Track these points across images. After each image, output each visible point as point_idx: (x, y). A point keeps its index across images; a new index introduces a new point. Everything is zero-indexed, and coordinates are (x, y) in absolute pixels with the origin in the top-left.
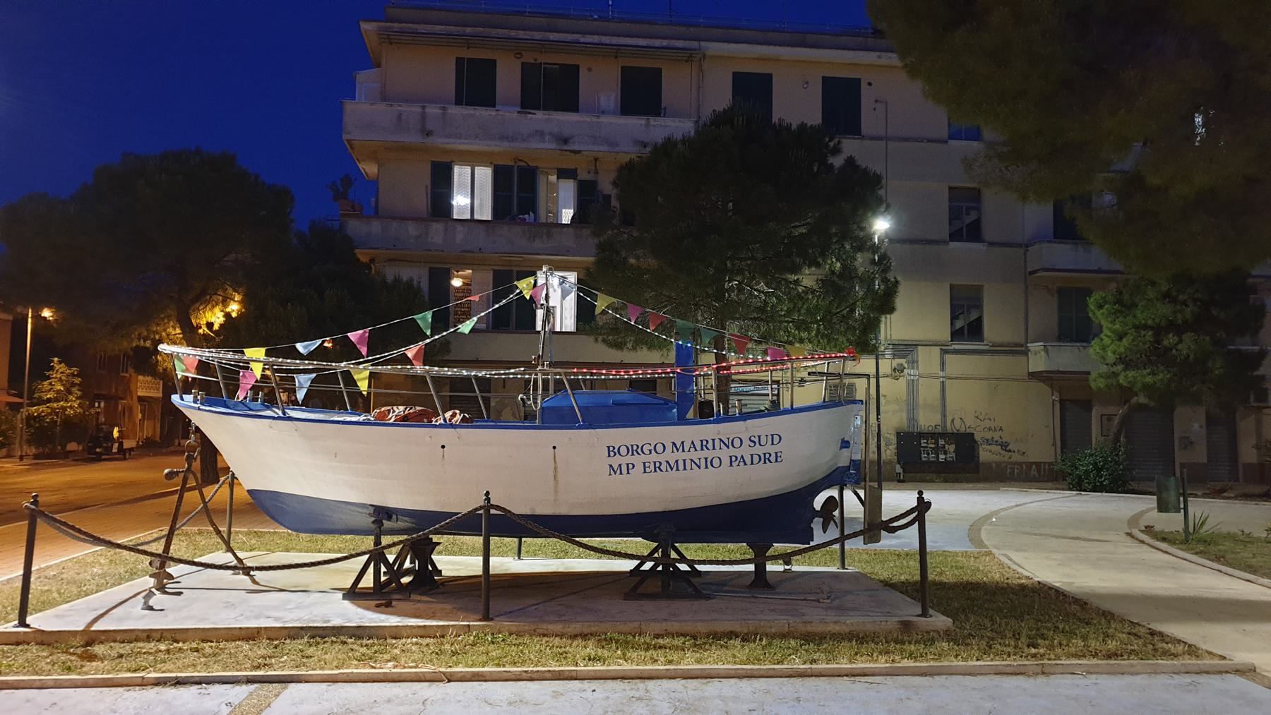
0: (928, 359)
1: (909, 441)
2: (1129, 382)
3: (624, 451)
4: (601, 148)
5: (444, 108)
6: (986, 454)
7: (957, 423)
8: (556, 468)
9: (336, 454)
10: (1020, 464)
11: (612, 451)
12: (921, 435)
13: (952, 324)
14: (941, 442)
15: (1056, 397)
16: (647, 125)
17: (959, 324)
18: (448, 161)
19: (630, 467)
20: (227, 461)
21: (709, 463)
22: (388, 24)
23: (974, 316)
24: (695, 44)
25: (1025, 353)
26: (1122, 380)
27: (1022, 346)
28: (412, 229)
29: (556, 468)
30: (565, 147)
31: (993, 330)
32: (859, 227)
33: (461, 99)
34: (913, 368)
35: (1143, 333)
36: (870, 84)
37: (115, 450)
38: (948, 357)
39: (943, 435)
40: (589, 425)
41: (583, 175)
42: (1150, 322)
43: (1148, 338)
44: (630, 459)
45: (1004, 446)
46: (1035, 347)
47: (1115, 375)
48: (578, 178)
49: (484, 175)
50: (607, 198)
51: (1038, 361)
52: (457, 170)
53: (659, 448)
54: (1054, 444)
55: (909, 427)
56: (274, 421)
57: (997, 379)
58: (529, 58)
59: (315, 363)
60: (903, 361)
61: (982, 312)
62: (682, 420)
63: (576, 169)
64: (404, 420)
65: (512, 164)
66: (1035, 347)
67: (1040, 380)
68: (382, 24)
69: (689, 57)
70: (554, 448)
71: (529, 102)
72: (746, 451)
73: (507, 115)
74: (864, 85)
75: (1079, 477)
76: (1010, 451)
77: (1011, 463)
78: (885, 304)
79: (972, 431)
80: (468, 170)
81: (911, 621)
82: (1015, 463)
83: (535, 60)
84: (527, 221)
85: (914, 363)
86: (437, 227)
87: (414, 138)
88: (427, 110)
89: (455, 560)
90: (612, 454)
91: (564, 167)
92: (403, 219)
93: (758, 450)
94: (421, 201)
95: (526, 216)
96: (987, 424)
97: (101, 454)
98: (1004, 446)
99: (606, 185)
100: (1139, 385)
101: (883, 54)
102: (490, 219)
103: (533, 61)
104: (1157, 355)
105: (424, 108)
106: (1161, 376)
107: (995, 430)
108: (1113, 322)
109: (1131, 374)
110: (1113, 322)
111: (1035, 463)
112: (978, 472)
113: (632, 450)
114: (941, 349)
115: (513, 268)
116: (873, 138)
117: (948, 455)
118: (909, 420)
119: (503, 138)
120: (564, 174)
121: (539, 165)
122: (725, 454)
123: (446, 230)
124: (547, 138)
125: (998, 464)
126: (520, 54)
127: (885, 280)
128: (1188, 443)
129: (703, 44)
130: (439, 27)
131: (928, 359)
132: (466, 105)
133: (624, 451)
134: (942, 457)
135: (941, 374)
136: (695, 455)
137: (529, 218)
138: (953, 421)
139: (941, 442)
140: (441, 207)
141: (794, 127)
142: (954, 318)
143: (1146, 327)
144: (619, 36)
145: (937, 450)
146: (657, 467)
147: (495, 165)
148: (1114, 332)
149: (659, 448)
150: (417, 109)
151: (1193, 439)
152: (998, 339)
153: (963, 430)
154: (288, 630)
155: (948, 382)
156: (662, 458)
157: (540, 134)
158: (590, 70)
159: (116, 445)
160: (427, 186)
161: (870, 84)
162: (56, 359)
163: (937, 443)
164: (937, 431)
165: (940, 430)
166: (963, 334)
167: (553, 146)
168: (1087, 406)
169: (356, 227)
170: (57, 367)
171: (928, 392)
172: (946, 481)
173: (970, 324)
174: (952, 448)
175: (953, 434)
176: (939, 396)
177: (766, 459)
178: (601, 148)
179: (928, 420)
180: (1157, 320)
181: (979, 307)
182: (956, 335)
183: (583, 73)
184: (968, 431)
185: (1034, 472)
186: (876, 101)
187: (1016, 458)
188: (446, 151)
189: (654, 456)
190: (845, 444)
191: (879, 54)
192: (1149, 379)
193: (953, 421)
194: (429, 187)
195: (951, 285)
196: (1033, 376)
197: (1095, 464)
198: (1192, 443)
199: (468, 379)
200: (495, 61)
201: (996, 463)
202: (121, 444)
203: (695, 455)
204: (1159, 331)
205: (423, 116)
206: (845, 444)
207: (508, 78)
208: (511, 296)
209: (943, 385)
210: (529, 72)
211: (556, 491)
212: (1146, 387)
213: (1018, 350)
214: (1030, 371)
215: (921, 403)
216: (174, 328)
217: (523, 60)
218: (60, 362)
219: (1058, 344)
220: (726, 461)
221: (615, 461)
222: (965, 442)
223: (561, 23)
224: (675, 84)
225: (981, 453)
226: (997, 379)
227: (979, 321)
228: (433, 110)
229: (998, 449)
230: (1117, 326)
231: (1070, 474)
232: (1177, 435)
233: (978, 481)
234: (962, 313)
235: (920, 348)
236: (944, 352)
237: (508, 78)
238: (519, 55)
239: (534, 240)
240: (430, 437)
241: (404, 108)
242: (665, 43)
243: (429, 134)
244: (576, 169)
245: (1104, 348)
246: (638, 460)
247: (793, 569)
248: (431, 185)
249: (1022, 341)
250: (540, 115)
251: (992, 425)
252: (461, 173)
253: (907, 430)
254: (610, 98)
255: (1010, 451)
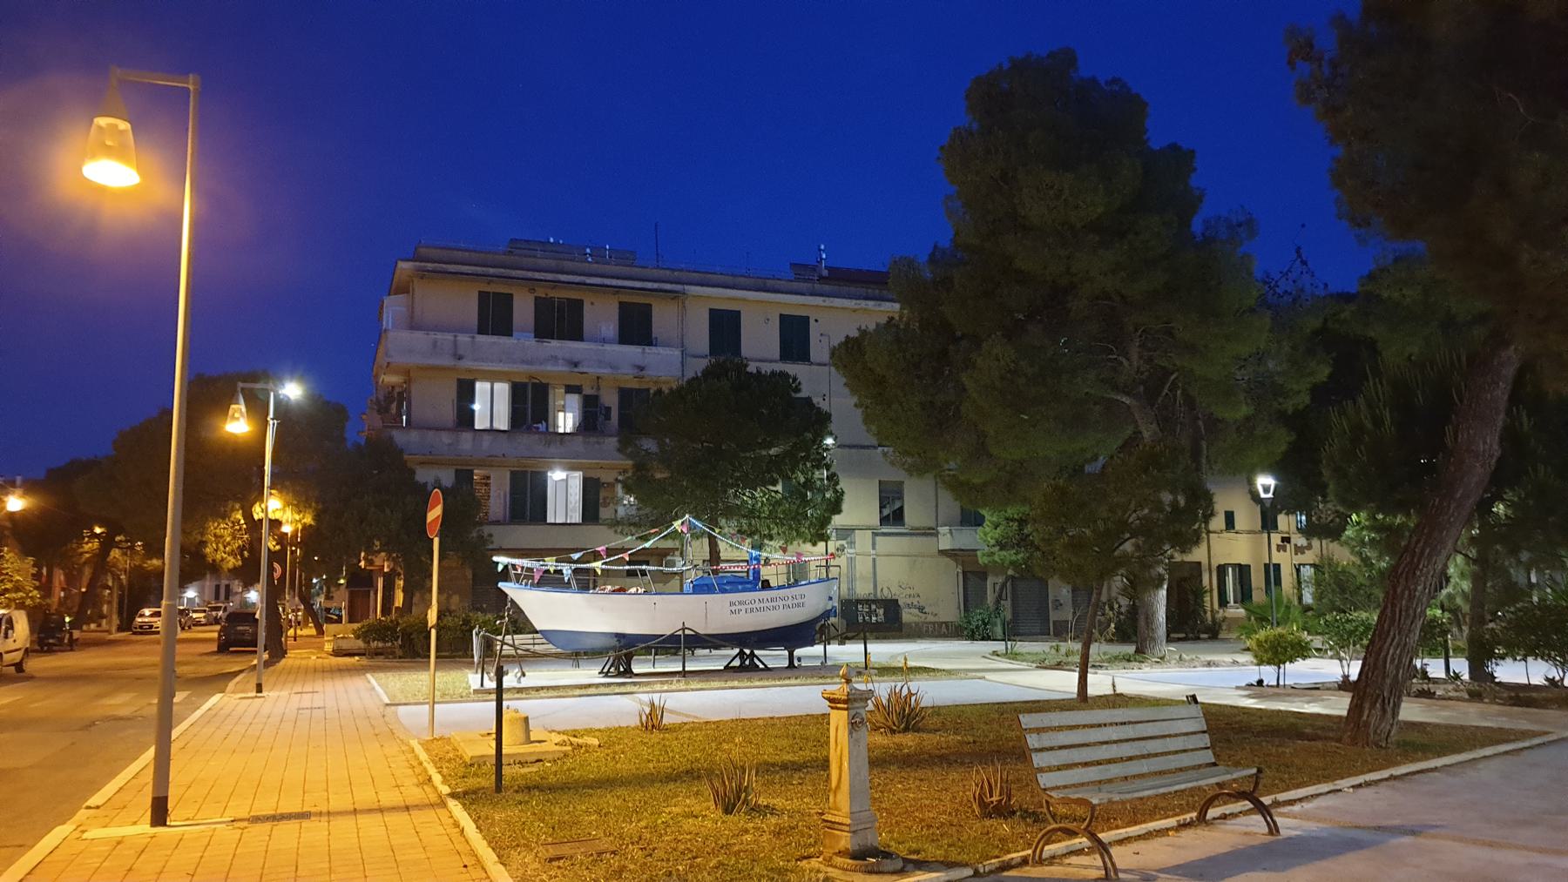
0: (863, 540)
1: (849, 607)
2: (1001, 560)
3: (737, 603)
4: (605, 371)
5: (473, 337)
6: (908, 616)
7: (886, 592)
10: (934, 623)
11: (732, 604)
12: (859, 601)
13: (881, 512)
14: (873, 607)
15: (960, 570)
16: (643, 352)
17: (886, 512)
18: (471, 378)
19: (740, 610)
20: (526, 613)
21: (774, 608)
22: (423, 264)
23: (897, 506)
24: (678, 287)
25: (936, 535)
26: (996, 558)
28: (446, 438)
30: (576, 370)
31: (914, 515)
33: (482, 330)
34: (851, 548)
35: (1011, 524)
36: (816, 321)
37: (66, 641)
38: (878, 538)
39: (875, 601)
40: (724, 591)
41: (588, 391)
42: (1016, 516)
43: (1014, 527)
44: (740, 607)
45: (921, 609)
46: (943, 530)
47: (993, 554)
48: (584, 393)
49: (503, 389)
50: (608, 409)
51: (945, 542)
52: (478, 385)
53: (753, 602)
54: (959, 608)
55: (849, 595)
57: (915, 556)
58: (541, 293)
60: (844, 542)
61: (903, 504)
62: (755, 590)
63: (581, 386)
64: (614, 592)
65: (527, 381)
66: (943, 530)
67: (948, 556)
68: (417, 264)
69: (674, 296)
71: (543, 331)
72: (790, 602)
73: (523, 342)
74: (812, 321)
75: (973, 631)
76: (925, 613)
77: (926, 623)
78: (835, 507)
79: (896, 597)
80: (487, 385)
81: (851, 859)
82: (930, 623)
83: (547, 295)
84: (541, 430)
85: (852, 544)
86: (466, 436)
87: (447, 361)
88: (458, 338)
91: (572, 383)
92: (437, 429)
93: (795, 601)
94: (448, 412)
95: (540, 425)
96: (908, 591)
97: (54, 645)
98: (921, 609)
99: (610, 399)
100: (1007, 562)
101: (827, 299)
102: (506, 428)
103: (544, 296)
104: (1023, 541)
105: (455, 336)
106: (1022, 555)
107: (914, 596)
108: (992, 515)
109: (1004, 553)
110: (992, 515)
111: (945, 623)
112: (901, 631)
113: (740, 603)
114: (873, 533)
115: (527, 469)
116: (819, 364)
117: (879, 617)
118: (849, 589)
119: (523, 362)
120: (570, 389)
121: (551, 382)
122: (781, 603)
123: (474, 439)
124: (560, 361)
125: (917, 624)
126: (534, 289)
127: (836, 491)
128: (1058, 605)
129: (686, 287)
130: (467, 267)
131: (863, 540)
132: (492, 334)
133: (737, 603)
134: (874, 618)
135: (873, 552)
136: (768, 604)
137: (542, 427)
138: (882, 590)
139: (873, 607)
140: (467, 418)
142: (882, 507)
143: (1013, 520)
144: (618, 278)
145: (870, 614)
146: (752, 610)
147: (513, 382)
148: (991, 522)
149: (753, 602)
150: (450, 337)
151: (1062, 602)
152: (917, 524)
153: (889, 597)
155: (878, 559)
156: (754, 606)
157: (554, 359)
158: (592, 304)
159: (67, 636)
160: (453, 401)
161: (816, 321)
162: (6, 549)
163: (870, 608)
164: (870, 598)
165: (872, 597)
166: (889, 520)
167: (564, 369)
168: (982, 575)
169: (399, 437)
170: (7, 557)
171: (863, 567)
172: (877, 638)
173: (894, 512)
174: (881, 611)
175: (882, 600)
176: (871, 570)
177: (798, 605)
178: (605, 371)
179: (863, 590)
180: (1020, 515)
181: (901, 498)
182: (884, 520)
183: (587, 307)
184: (894, 598)
185: (944, 630)
186: (822, 335)
187: (931, 618)
188: (469, 371)
189: (751, 606)
190: (830, 598)
192: (1014, 558)
193: (882, 590)
194: (455, 402)
195: (880, 481)
196: (943, 553)
197: (983, 620)
198: (1061, 605)
199: (635, 570)
200: (511, 295)
201: (915, 623)
202: (71, 634)
203: (768, 604)
204: (1022, 522)
205: (455, 342)
206: (830, 598)
207: (523, 309)
209: (874, 560)
210: (541, 306)
211: (706, 623)
212: (1012, 563)
213: (930, 532)
215: (858, 575)
217: (535, 294)
218: (9, 552)
219: (960, 528)
220: (781, 607)
221: (733, 608)
222: (891, 606)
223: (569, 265)
224: (663, 317)
225: (904, 614)
226: (915, 556)
227: (901, 509)
228: (463, 339)
229: (916, 611)
230: (994, 519)
231: (966, 628)
232: (1051, 598)
233: (902, 638)
234: (888, 503)
235: (857, 531)
236: (875, 534)
237: (523, 309)
238: (532, 290)
239: (549, 447)
241: (439, 336)
242: (656, 285)
243: (460, 358)
244: (581, 386)
245: (985, 534)
246: (743, 607)
247: (803, 665)
248: (458, 401)
249: (933, 525)
250: (555, 343)
251: (912, 592)
252: (481, 387)
253: (847, 597)
254: (610, 328)
255: (925, 613)
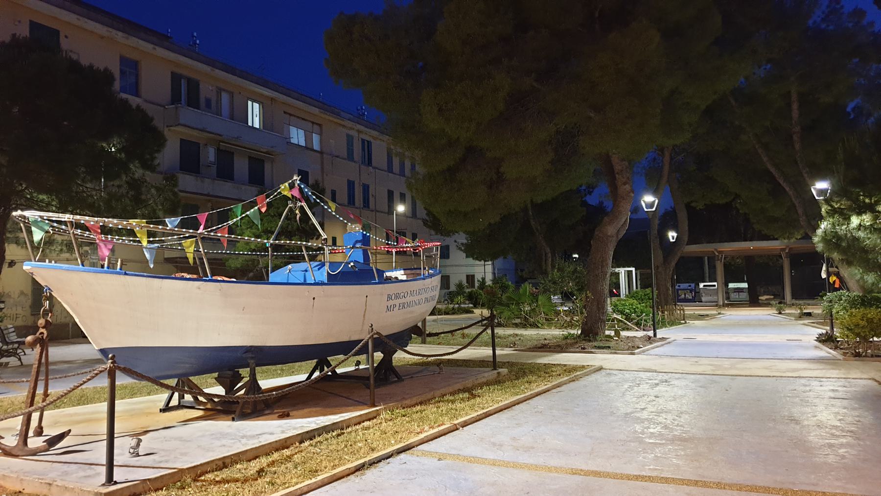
8: (366, 309)
9: (244, 308)
27: (438, 247)
29: (366, 309)
32: (826, 235)
36: (66, 37)
56: (206, 283)
59: (191, 231)
70: (314, 299)
89: (349, 368)
90: (389, 299)
141: (102, 70)
154: (301, 435)
161: (66, 37)
191: (78, 17)
208: (272, 197)
214: (165, 257)
216: (21, 185)
240: (308, 292)
